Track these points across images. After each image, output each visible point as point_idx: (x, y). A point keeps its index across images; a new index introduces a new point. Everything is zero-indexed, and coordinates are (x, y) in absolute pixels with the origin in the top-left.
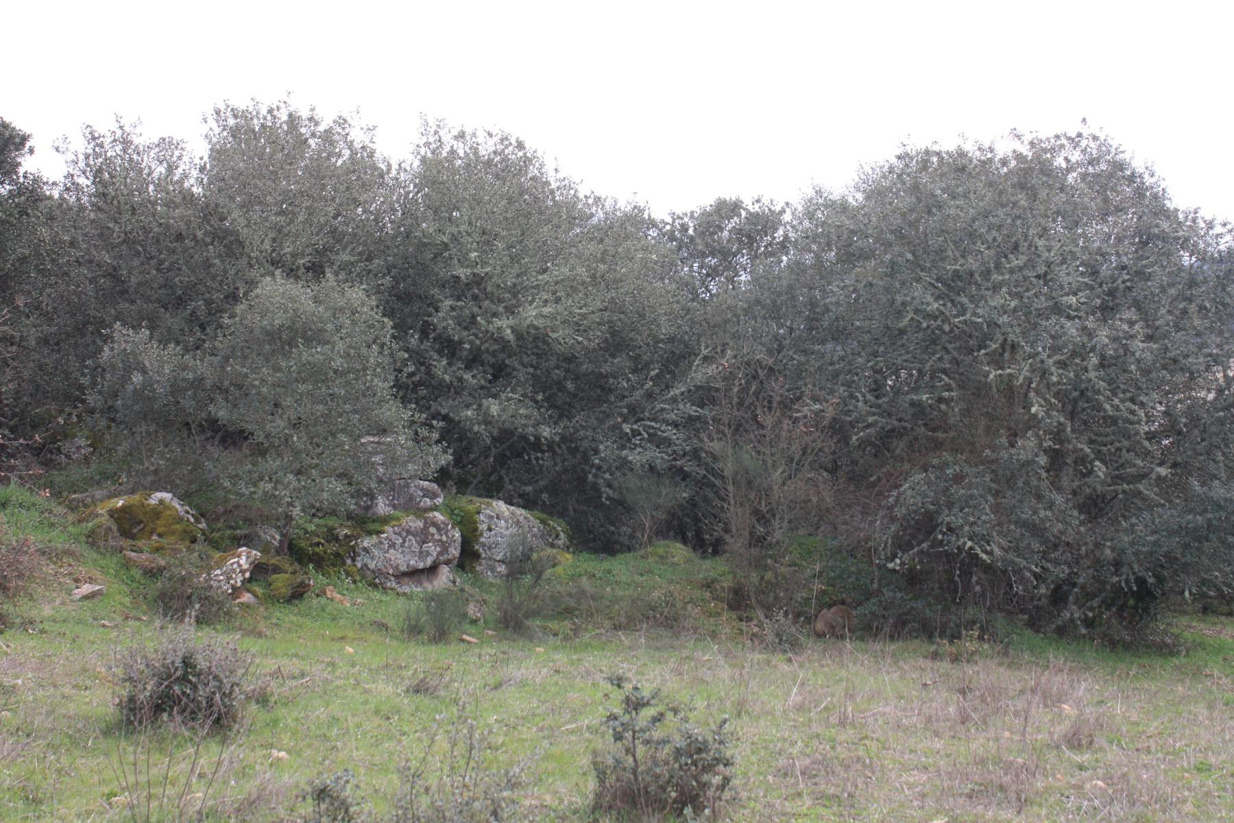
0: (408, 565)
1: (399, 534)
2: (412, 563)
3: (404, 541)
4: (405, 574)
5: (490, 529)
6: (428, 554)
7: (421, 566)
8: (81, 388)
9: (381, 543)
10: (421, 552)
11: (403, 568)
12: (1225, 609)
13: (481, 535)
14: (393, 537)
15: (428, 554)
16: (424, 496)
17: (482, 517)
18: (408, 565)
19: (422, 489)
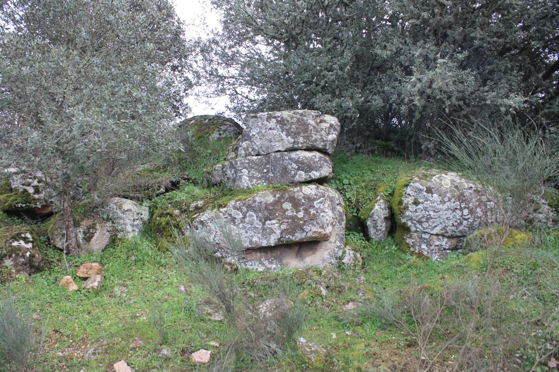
0: (251, 242)
1: (240, 209)
2: (254, 239)
3: (245, 217)
4: (249, 250)
5: (416, 203)
6: (272, 232)
7: (264, 243)
8: (513, 116)
9: (217, 217)
10: (264, 229)
11: (247, 244)
12: (466, 160)
13: (406, 208)
14: (233, 212)
15: (272, 232)
16: (299, 169)
17: (409, 190)
18: (251, 242)
19: (297, 162)
